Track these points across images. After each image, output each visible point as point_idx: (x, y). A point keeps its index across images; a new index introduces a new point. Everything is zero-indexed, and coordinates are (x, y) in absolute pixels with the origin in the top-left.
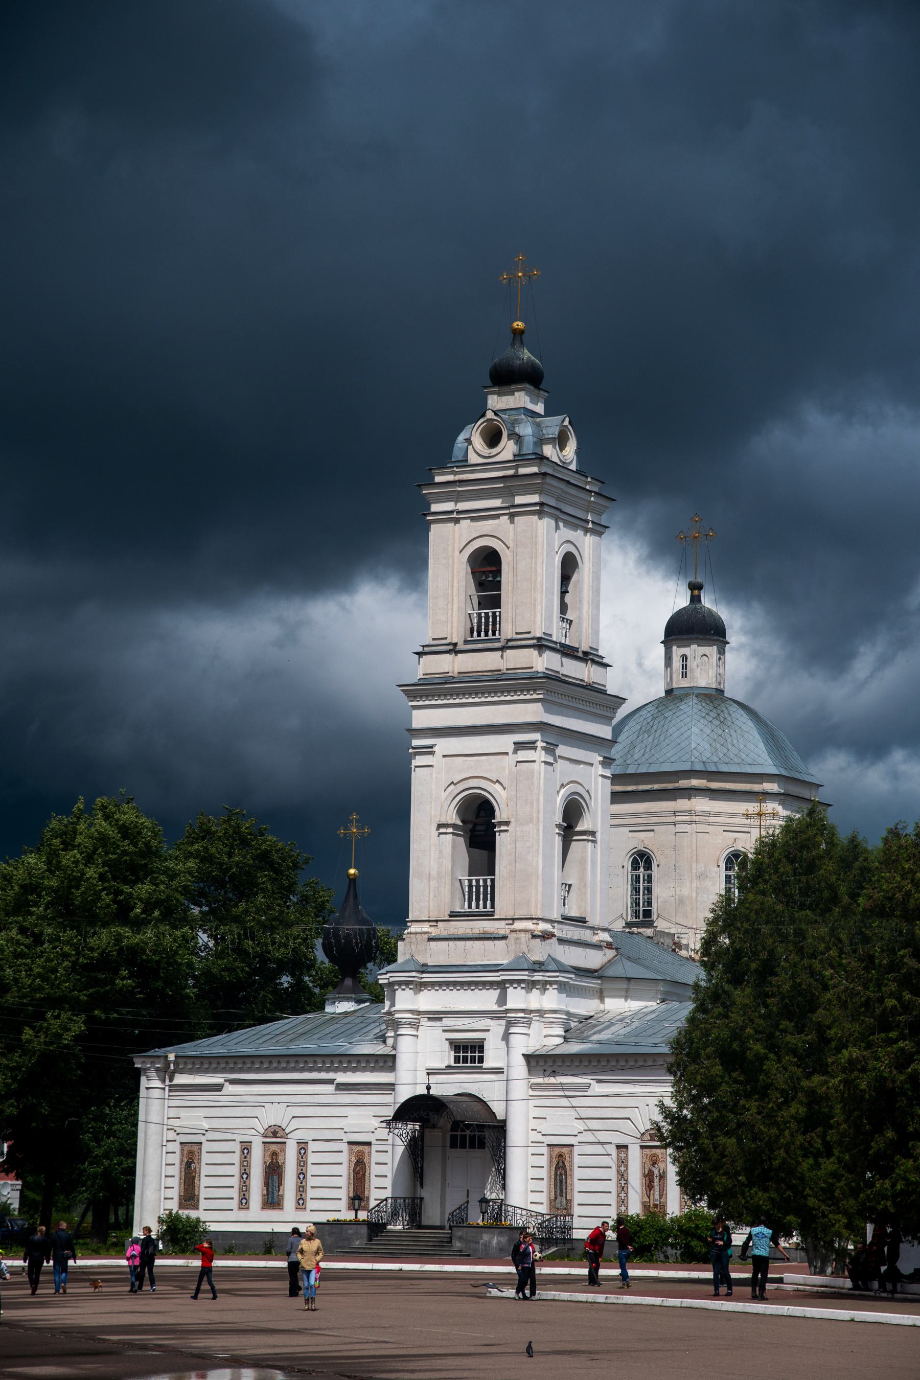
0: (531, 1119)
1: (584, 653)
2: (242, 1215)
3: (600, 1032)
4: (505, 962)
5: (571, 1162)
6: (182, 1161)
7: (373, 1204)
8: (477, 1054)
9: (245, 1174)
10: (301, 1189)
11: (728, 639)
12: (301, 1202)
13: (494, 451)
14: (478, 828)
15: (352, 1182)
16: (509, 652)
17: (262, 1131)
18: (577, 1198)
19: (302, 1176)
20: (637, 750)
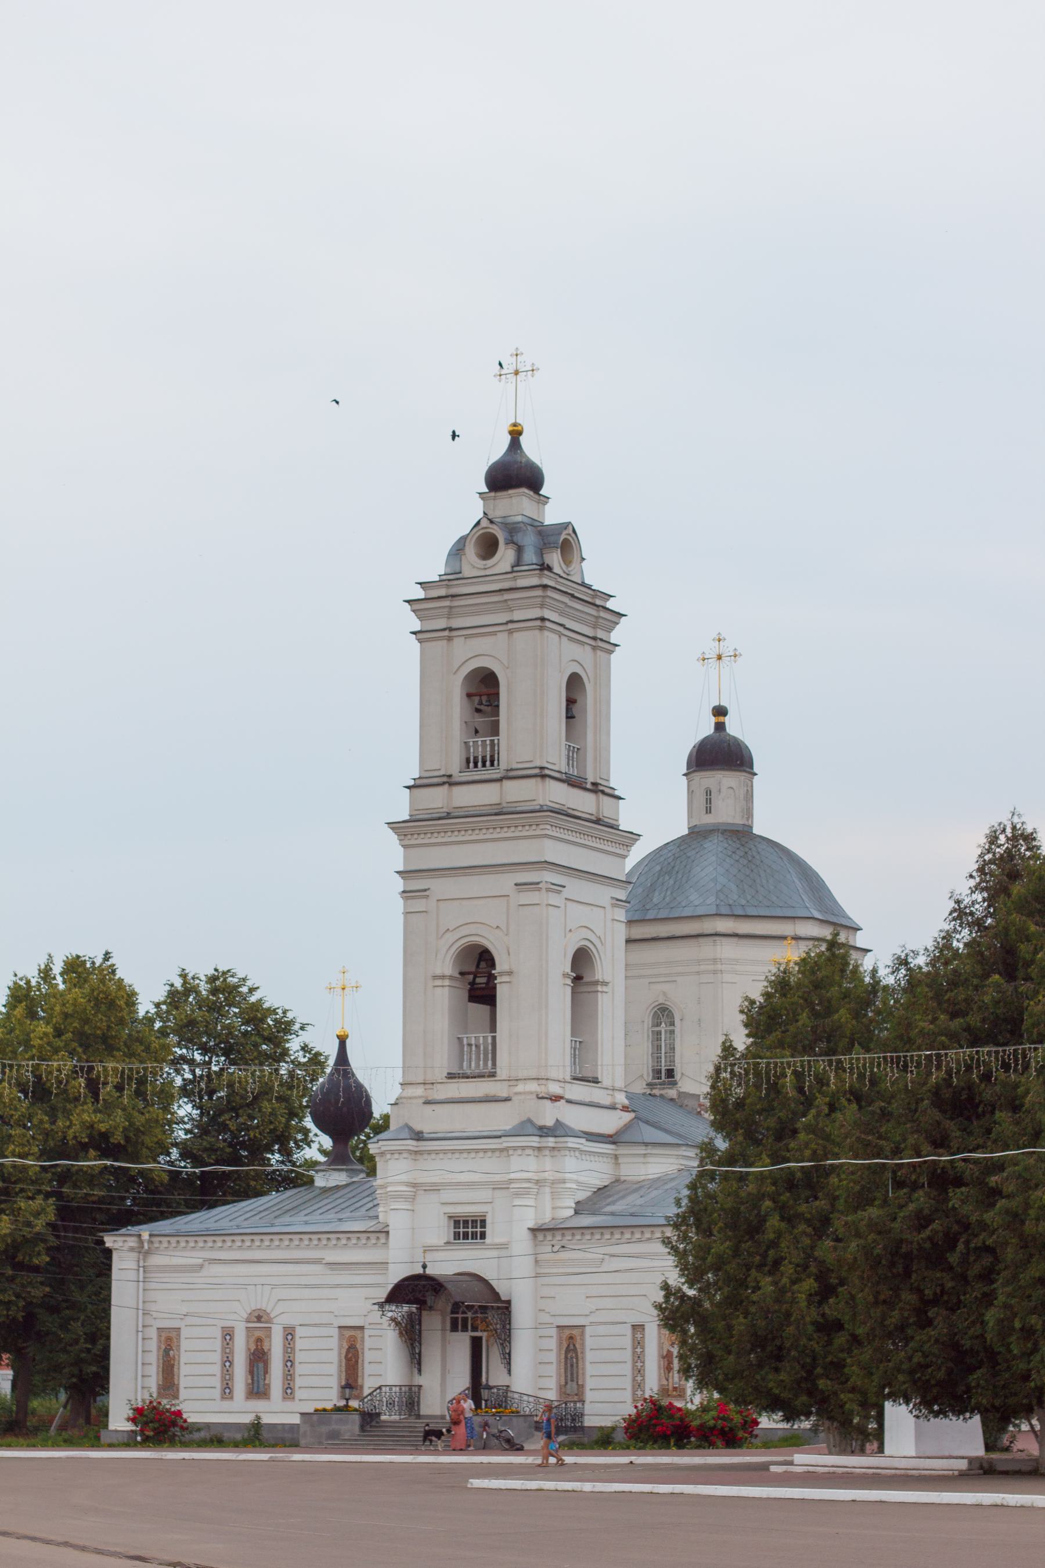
0: (540, 1296)
1: (593, 784)
2: (226, 1405)
3: (613, 1203)
4: (508, 1128)
5: (583, 1344)
6: (159, 1348)
7: (366, 1391)
8: (479, 1230)
9: (227, 1361)
10: (289, 1377)
11: (756, 770)
12: (289, 1391)
13: (490, 562)
14: (478, 980)
15: (343, 1369)
16: (507, 784)
17: (245, 1316)
18: (590, 1383)
19: (289, 1364)
20: (657, 893)
